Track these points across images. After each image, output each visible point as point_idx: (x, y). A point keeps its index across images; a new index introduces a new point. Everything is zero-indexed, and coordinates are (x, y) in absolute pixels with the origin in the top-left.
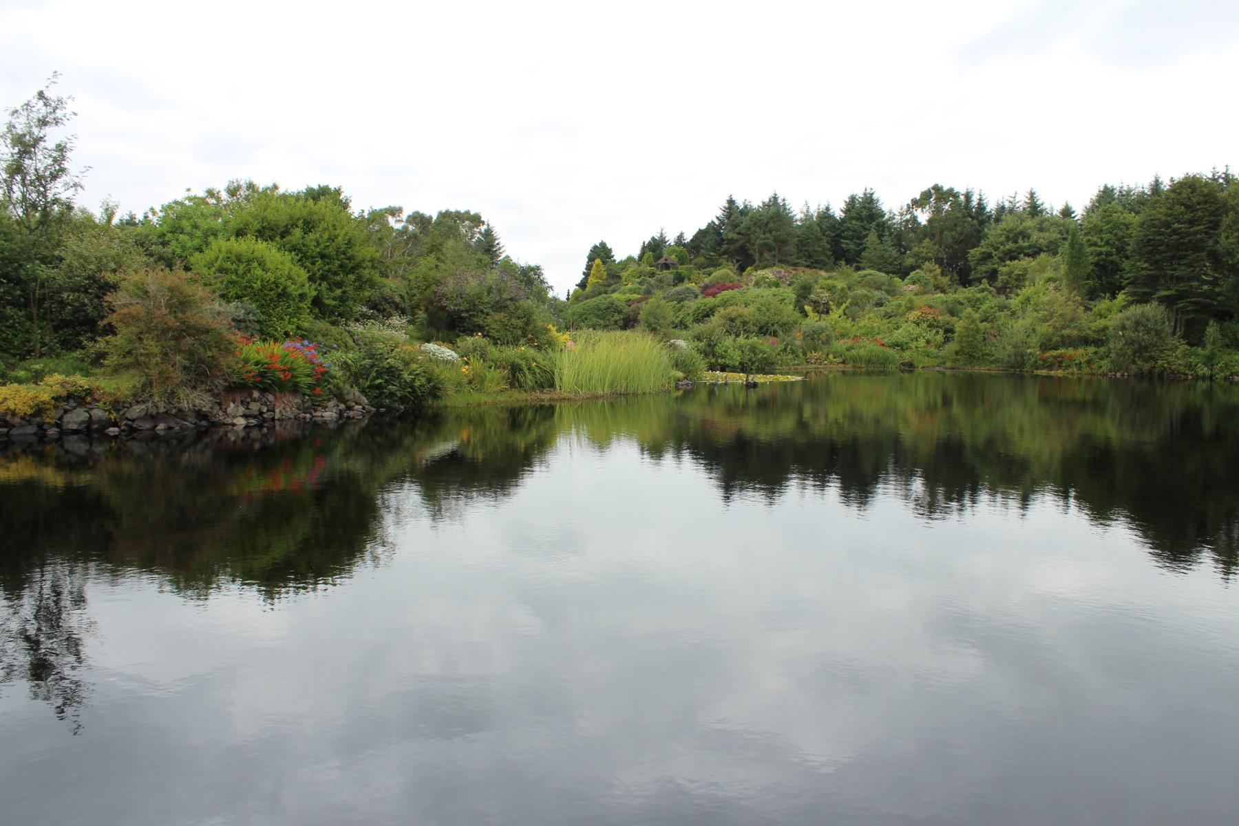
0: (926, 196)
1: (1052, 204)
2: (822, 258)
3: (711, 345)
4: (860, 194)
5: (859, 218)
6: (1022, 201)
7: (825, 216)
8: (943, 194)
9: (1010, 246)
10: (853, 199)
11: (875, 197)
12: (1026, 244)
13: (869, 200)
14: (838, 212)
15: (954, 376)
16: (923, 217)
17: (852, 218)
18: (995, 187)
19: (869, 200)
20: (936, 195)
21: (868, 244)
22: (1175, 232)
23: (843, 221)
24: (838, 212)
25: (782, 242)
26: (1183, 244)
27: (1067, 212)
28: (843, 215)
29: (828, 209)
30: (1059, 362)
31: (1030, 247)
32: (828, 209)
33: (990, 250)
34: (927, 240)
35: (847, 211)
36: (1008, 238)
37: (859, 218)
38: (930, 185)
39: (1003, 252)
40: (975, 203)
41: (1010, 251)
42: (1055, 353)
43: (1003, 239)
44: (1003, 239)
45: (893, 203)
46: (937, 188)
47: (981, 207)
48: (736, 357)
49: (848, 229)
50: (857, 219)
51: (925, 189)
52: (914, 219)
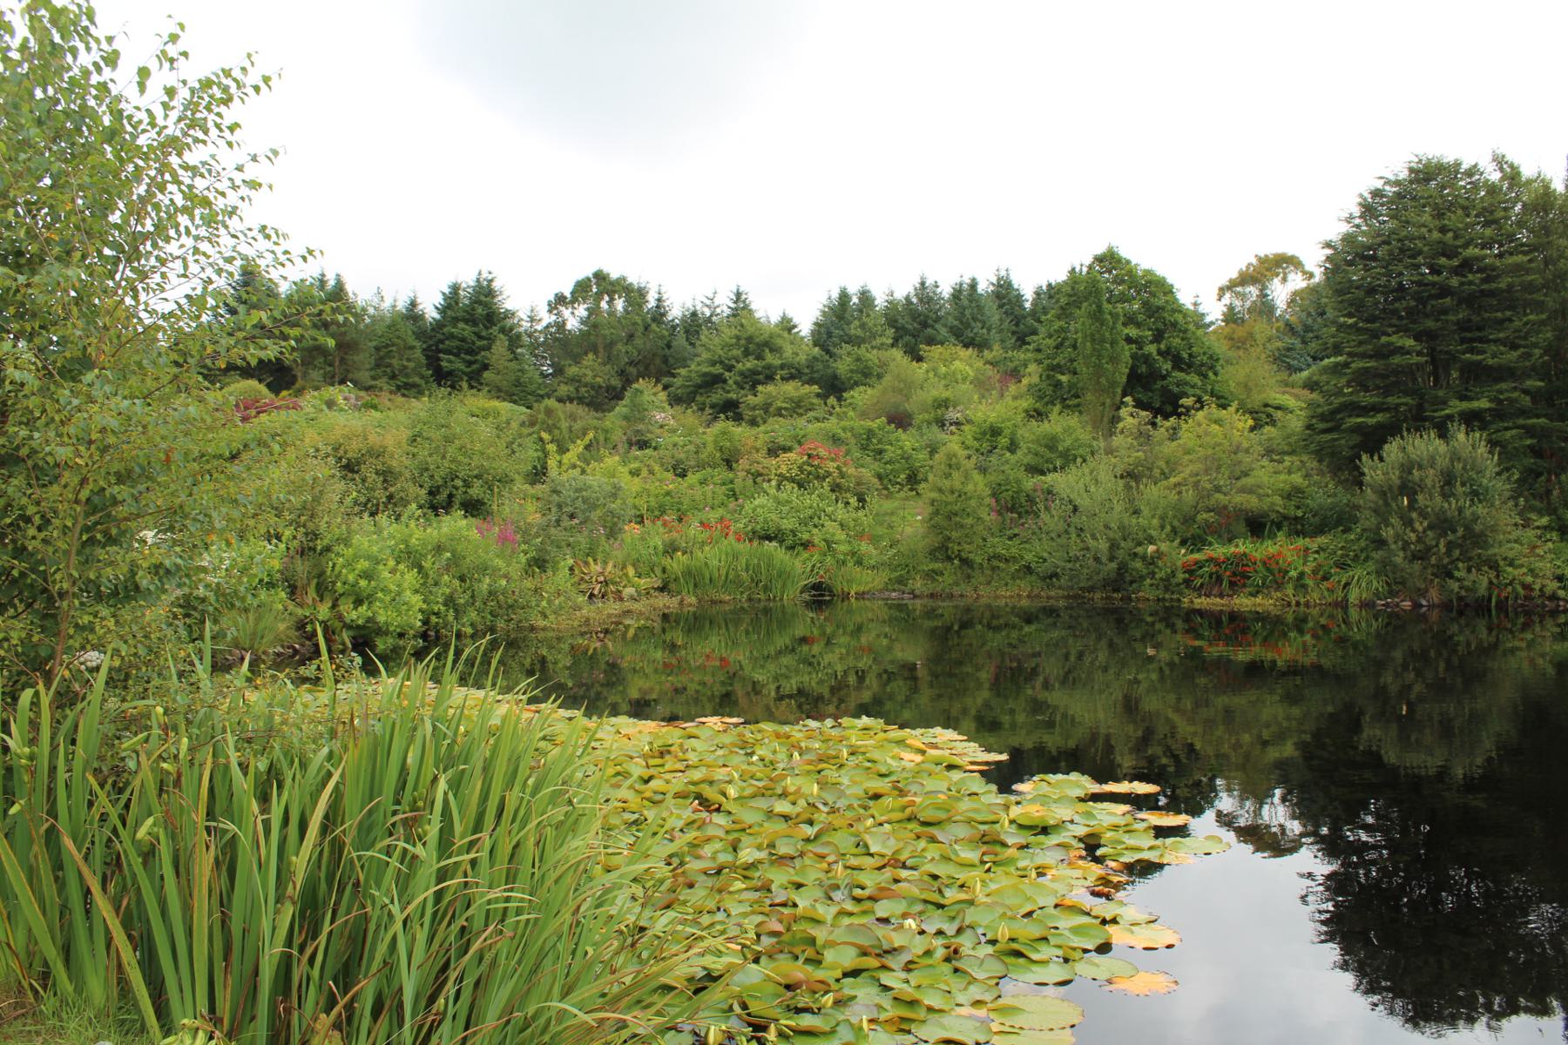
0: (582, 288)
1: (767, 310)
2: (417, 380)
3: (311, 549)
4: (468, 279)
5: (471, 319)
6: (724, 303)
7: (412, 314)
8: (612, 283)
9: (750, 363)
10: (455, 288)
11: (496, 285)
12: (777, 362)
13: (485, 293)
14: (430, 307)
15: (930, 613)
16: (573, 319)
17: (456, 320)
18: (683, 285)
19: (485, 293)
20: (599, 286)
21: (493, 361)
22: (1467, 265)
23: (438, 325)
24: (430, 307)
25: (345, 346)
26: (1492, 294)
27: (787, 325)
28: (438, 316)
29: (413, 304)
30: (1237, 575)
31: (782, 367)
32: (413, 304)
33: (718, 369)
34: (591, 356)
35: (443, 310)
36: (747, 353)
37: (471, 319)
38: (589, 272)
39: (741, 373)
40: (652, 303)
41: (754, 372)
42: (1220, 551)
43: (737, 352)
44: (737, 352)
45: (528, 297)
46: (600, 276)
47: (659, 314)
48: (402, 602)
49: (452, 336)
50: (466, 321)
51: (581, 276)
52: (561, 326)
